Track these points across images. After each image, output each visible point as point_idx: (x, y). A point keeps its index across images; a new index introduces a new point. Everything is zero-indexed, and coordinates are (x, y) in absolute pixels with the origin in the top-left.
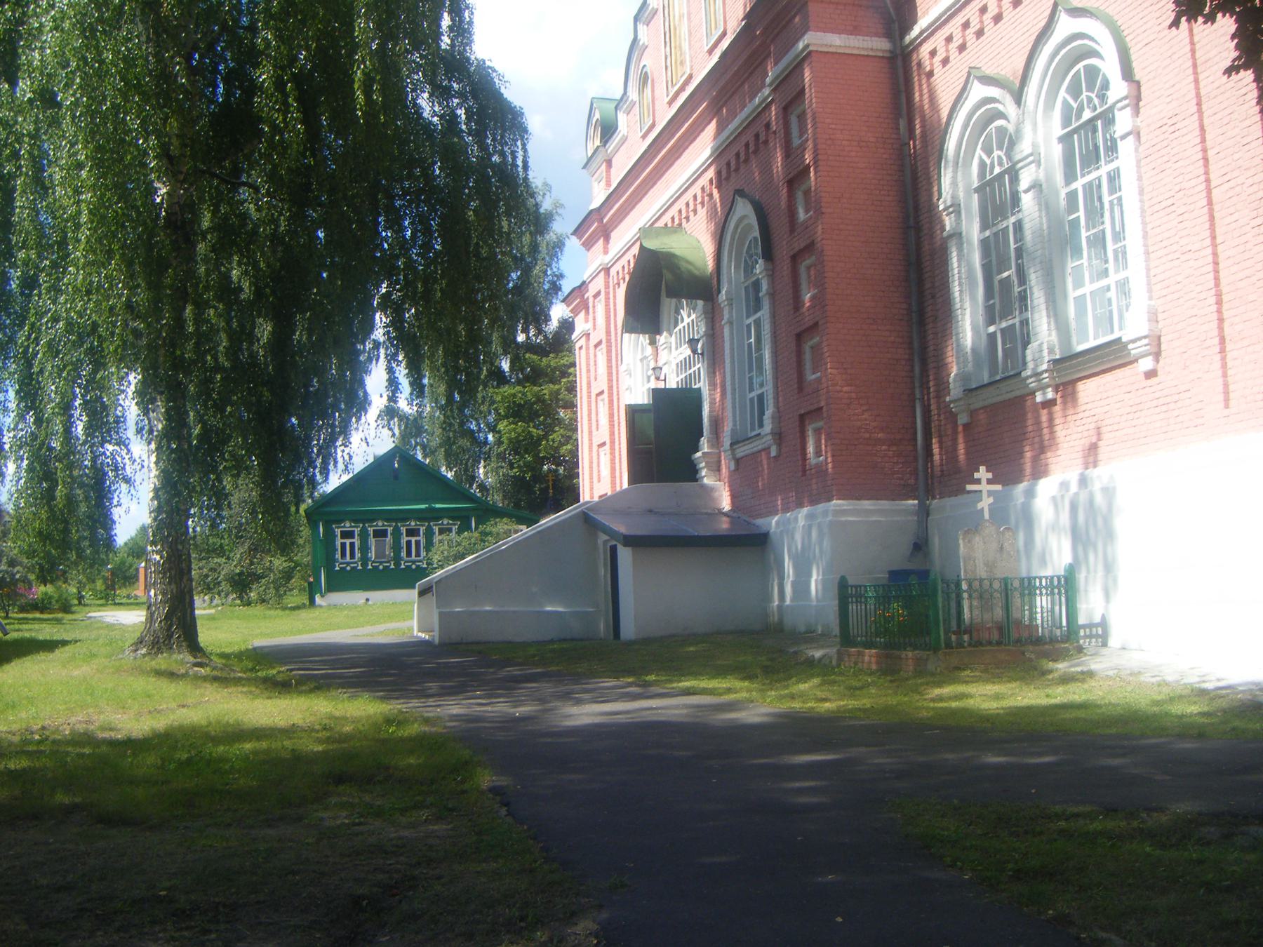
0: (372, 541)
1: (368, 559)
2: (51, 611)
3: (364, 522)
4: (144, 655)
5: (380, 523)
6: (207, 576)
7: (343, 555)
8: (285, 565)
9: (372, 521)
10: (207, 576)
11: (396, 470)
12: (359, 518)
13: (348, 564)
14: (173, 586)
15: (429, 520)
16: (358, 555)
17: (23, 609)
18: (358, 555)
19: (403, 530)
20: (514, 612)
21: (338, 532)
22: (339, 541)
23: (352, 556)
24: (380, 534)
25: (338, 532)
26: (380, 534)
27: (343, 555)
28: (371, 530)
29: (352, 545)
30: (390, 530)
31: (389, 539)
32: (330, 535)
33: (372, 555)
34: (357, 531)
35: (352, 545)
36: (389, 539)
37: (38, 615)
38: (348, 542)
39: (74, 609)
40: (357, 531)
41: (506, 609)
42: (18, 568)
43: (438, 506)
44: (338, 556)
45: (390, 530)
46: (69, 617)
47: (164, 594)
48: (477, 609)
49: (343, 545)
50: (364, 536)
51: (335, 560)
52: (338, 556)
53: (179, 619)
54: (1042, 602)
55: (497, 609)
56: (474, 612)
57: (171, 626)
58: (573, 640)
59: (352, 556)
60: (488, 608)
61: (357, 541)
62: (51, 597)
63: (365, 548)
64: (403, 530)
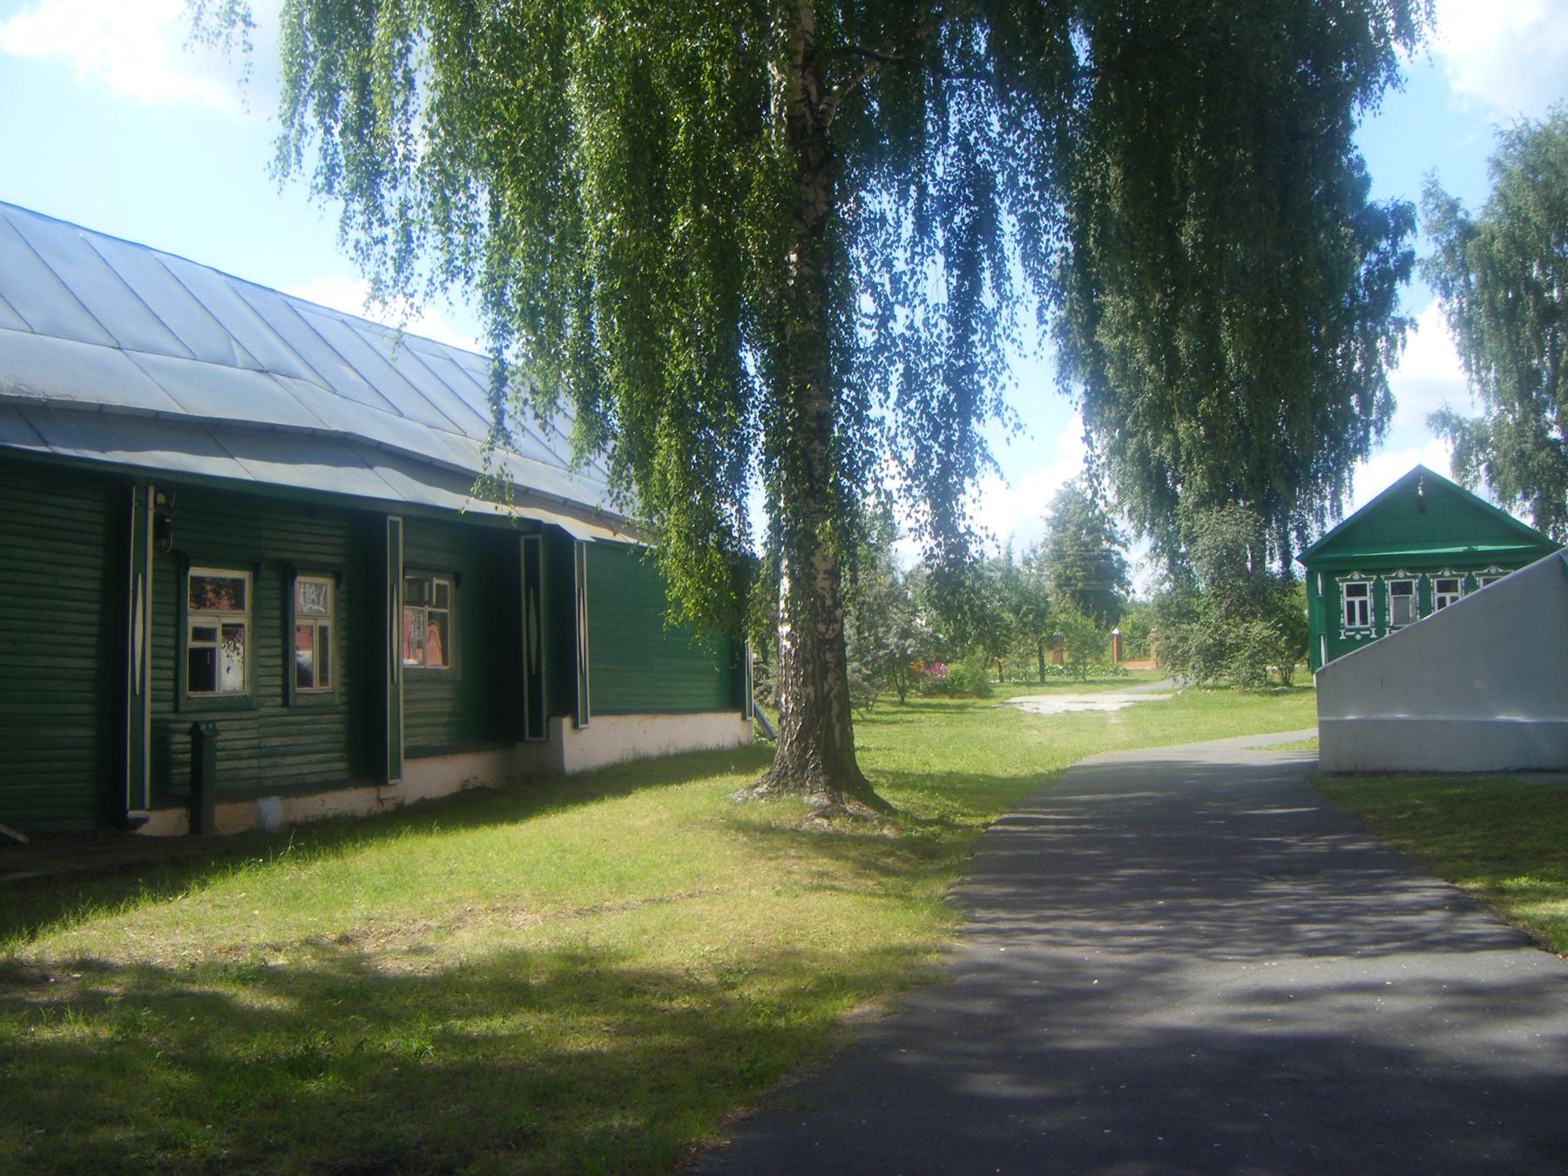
0: (1390, 600)
1: (1385, 624)
2: (963, 695)
3: (1378, 571)
4: (762, 796)
5: (1401, 574)
6: (1176, 648)
7: (1351, 619)
8: (1266, 633)
9: (1391, 570)
10: (1176, 648)
11: (1419, 498)
12: (1369, 567)
13: (1358, 631)
14: (810, 689)
15: (1470, 567)
16: (1371, 618)
17: (929, 693)
18: (1371, 618)
19: (1434, 583)
20: (1443, 723)
21: (1343, 586)
22: (1345, 600)
23: (1364, 619)
24: (1402, 589)
25: (1343, 586)
26: (1402, 589)
27: (1351, 619)
28: (1388, 583)
29: (1363, 605)
30: (1415, 583)
31: (1414, 596)
32: (1332, 593)
33: (1390, 618)
34: (1369, 585)
35: (1363, 605)
36: (1414, 596)
37: (947, 700)
38: (1357, 600)
39: (996, 691)
40: (1369, 585)
41: (1428, 717)
42: (910, 641)
43: (1481, 548)
44: (1344, 620)
45: (1415, 583)
46: (984, 702)
47: (796, 701)
48: (1383, 716)
49: (1351, 605)
50: (1379, 591)
51: (1340, 626)
52: (1344, 620)
53: (817, 740)
54: (852, 1001)
55: (1415, 717)
56: (1376, 724)
57: (805, 750)
58: (1540, 770)
59: (1364, 619)
60: (1401, 716)
61: (1369, 599)
62: (962, 678)
63: (1380, 609)
64: (1434, 583)
